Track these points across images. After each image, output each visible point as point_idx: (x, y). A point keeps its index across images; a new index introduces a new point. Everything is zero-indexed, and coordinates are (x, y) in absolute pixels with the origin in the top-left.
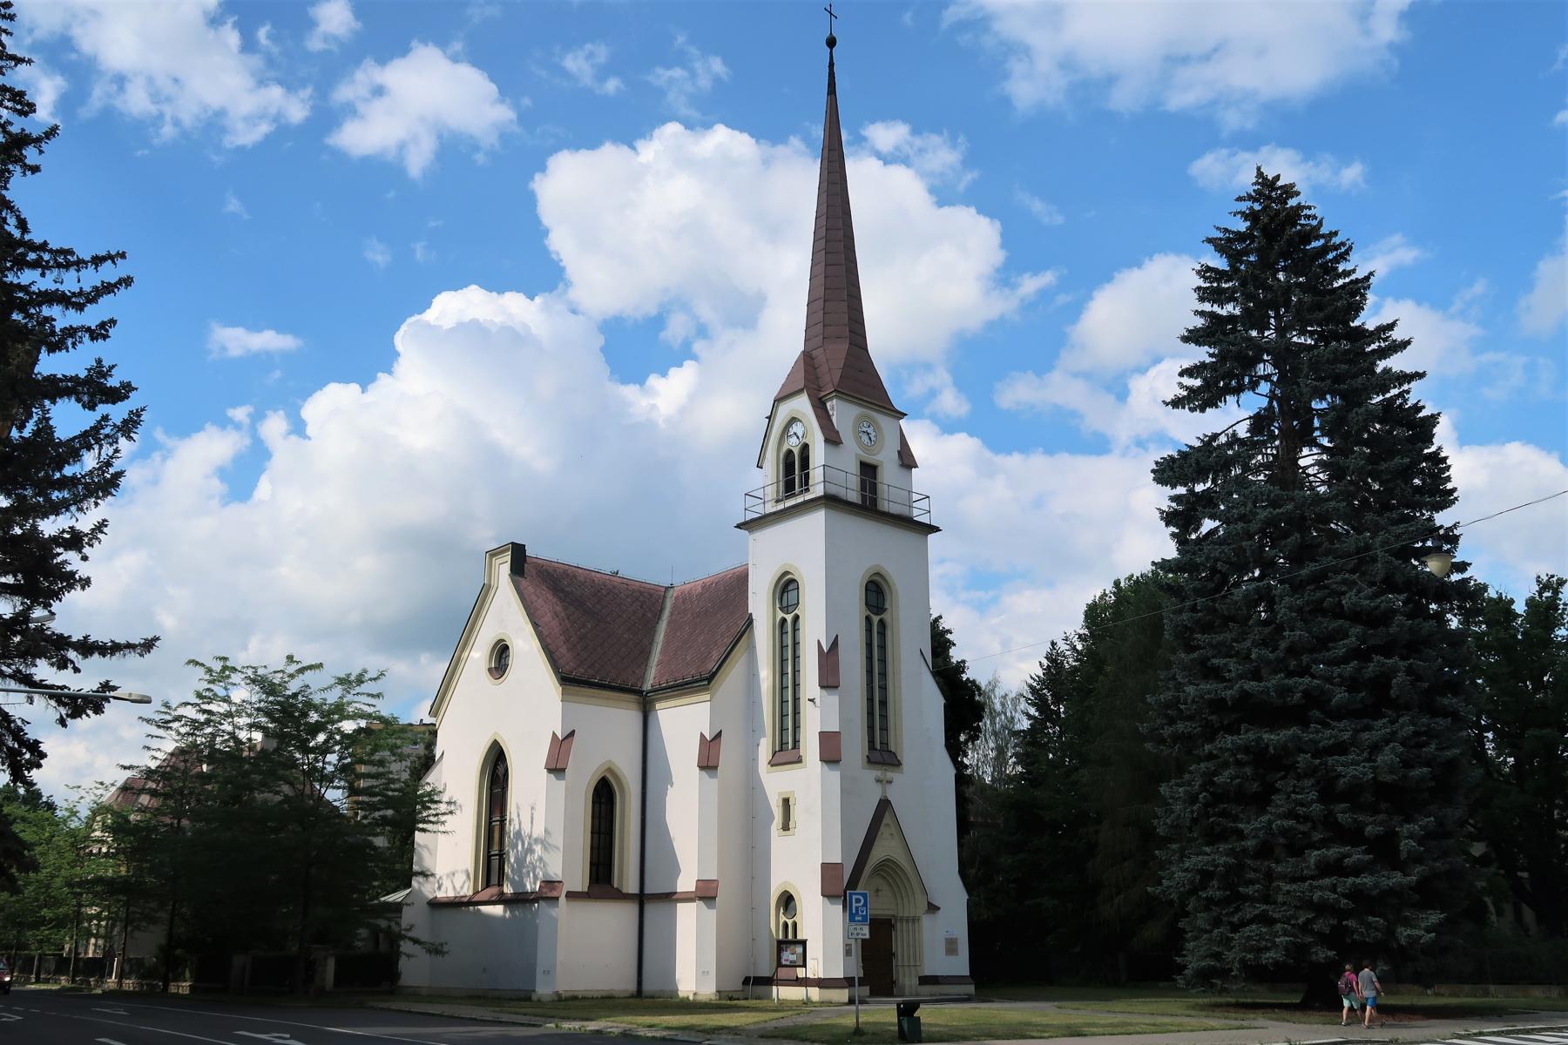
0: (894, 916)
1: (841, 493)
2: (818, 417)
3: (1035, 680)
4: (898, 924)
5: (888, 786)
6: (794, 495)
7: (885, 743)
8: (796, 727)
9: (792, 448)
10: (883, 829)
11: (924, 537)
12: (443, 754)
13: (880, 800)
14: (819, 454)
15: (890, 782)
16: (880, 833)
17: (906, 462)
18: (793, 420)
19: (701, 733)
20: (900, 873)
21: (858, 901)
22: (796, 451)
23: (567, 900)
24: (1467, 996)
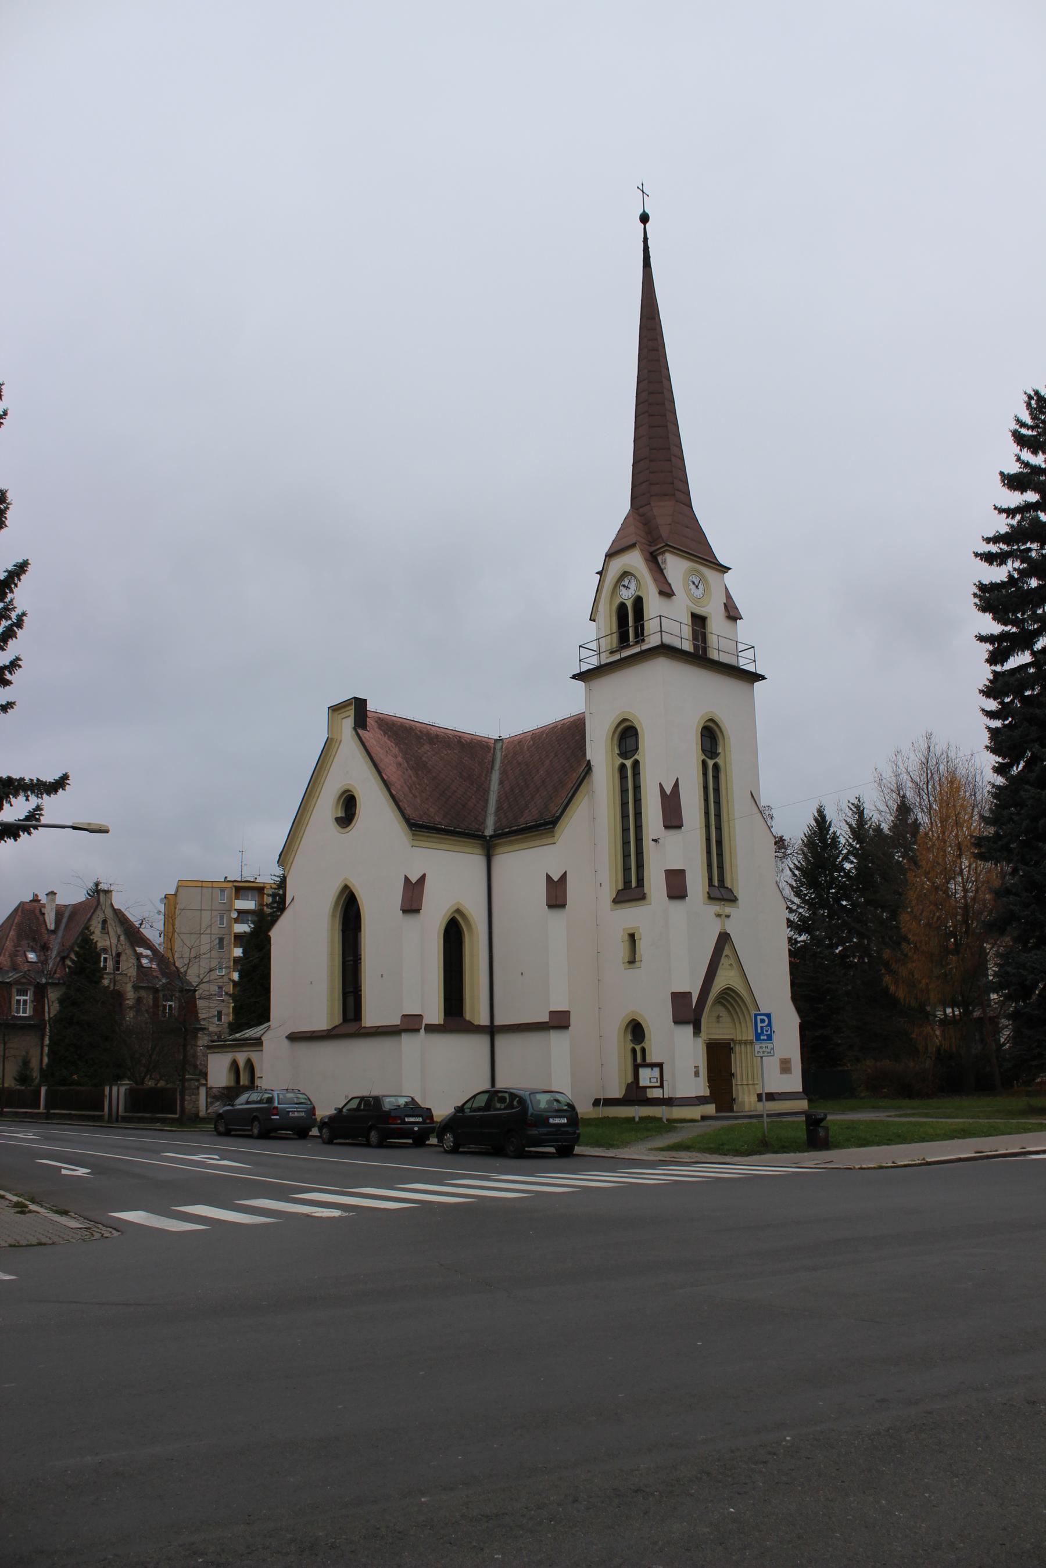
0: (732, 1040)
1: (676, 643)
2: (651, 570)
4: (737, 1047)
5: (727, 920)
6: (628, 646)
7: (721, 880)
10: (723, 960)
11: (752, 685)
12: (293, 899)
13: (720, 934)
14: (654, 605)
15: (728, 916)
16: (721, 964)
18: (625, 574)
19: (547, 874)
20: (741, 1003)
21: (762, 1021)
22: (629, 604)
23: (425, 1033)
24: (942, 1122)
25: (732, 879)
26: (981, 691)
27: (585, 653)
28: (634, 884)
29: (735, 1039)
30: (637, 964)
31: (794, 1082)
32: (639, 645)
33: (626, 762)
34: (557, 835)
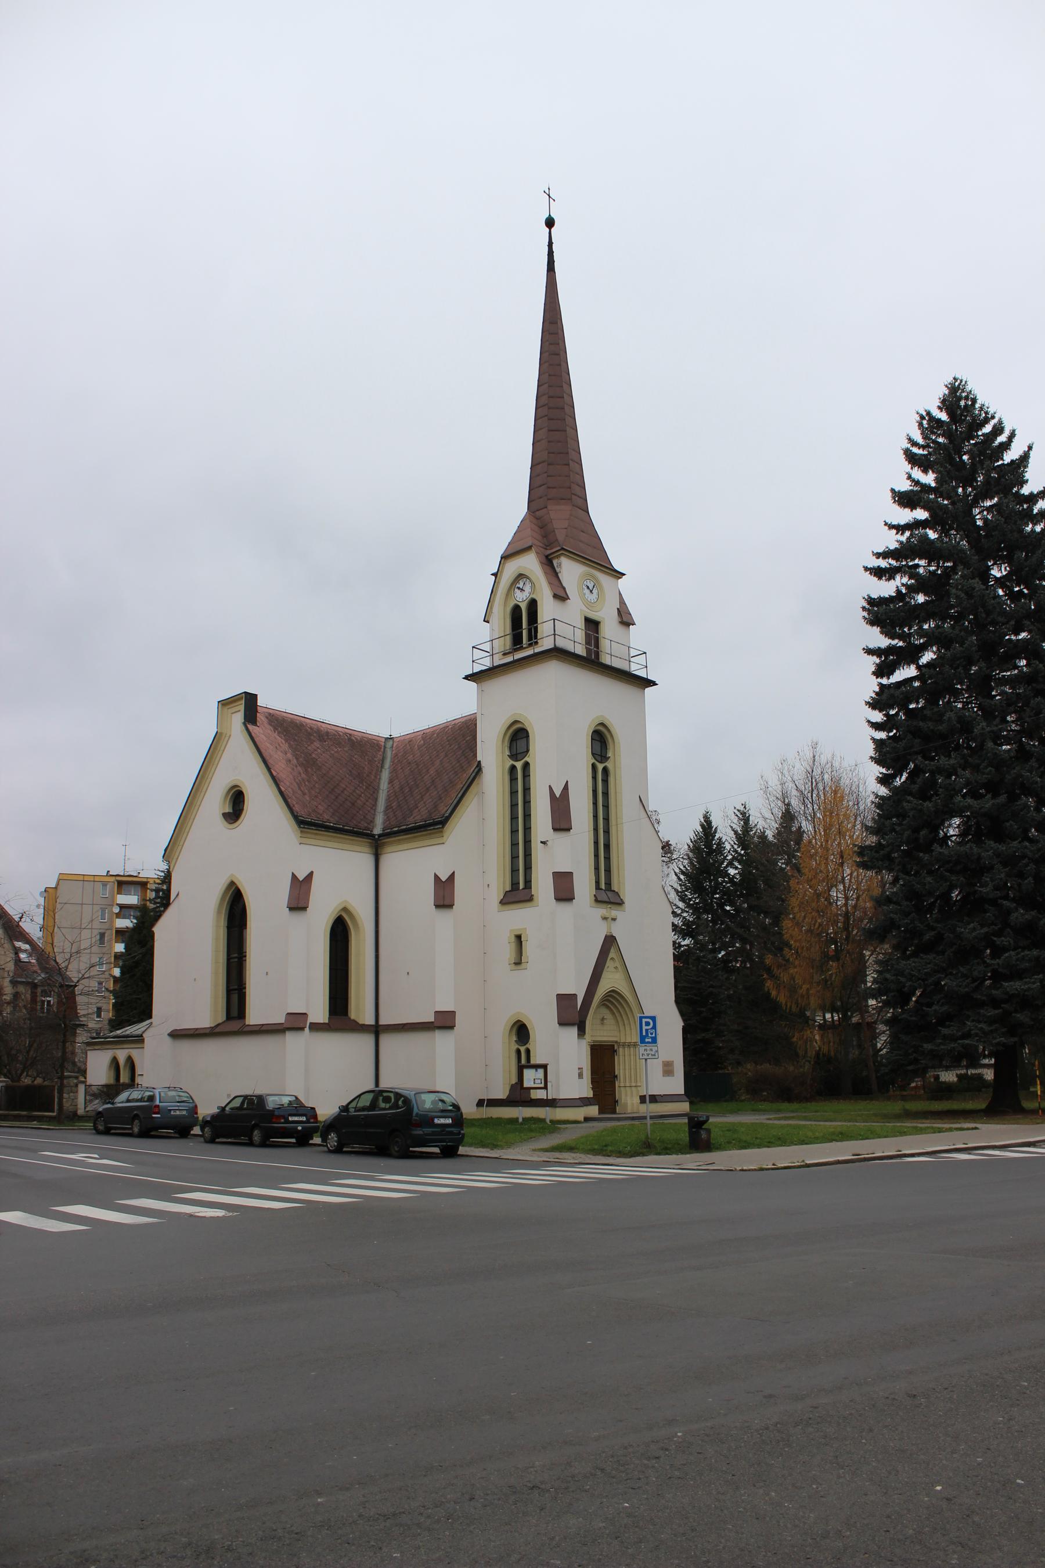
0: (616, 1042)
1: (569, 646)
3: (692, 842)
4: (621, 1049)
6: (521, 648)
7: (608, 884)
8: (528, 867)
9: (520, 604)
10: (609, 963)
12: (178, 895)
13: (606, 936)
14: (547, 609)
15: (614, 919)
16: (606, 967)
17: (625, 619)
18: (520, 576)
19: (435, 874)
21: (647, 1024)
22: (524, 607)
23: (310, 1032)
25: (619, 883)
26: (867, 703)
27: (478, 654)
28: (521, 886)
29: (619, 1041)
30: (523, 966)
31: (676, 1085)
32: (532, 648)
33: (516, 764)
34: (446, 835)
